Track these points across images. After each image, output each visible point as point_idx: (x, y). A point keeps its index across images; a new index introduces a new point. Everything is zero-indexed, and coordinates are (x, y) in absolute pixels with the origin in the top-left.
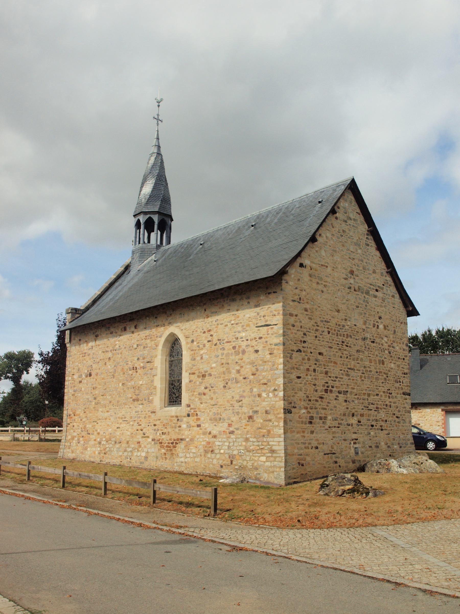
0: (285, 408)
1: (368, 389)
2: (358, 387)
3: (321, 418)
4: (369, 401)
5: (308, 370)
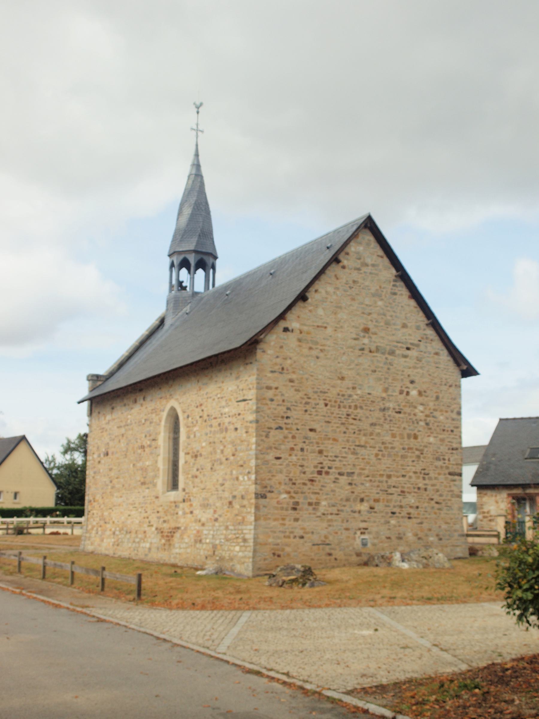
0: (257, 492)
1: (388, 470)
2: (371, 468)
3: (310, 504)
4: (389, 484)
5: (292, 449)
